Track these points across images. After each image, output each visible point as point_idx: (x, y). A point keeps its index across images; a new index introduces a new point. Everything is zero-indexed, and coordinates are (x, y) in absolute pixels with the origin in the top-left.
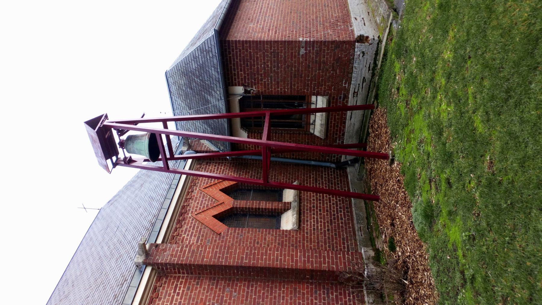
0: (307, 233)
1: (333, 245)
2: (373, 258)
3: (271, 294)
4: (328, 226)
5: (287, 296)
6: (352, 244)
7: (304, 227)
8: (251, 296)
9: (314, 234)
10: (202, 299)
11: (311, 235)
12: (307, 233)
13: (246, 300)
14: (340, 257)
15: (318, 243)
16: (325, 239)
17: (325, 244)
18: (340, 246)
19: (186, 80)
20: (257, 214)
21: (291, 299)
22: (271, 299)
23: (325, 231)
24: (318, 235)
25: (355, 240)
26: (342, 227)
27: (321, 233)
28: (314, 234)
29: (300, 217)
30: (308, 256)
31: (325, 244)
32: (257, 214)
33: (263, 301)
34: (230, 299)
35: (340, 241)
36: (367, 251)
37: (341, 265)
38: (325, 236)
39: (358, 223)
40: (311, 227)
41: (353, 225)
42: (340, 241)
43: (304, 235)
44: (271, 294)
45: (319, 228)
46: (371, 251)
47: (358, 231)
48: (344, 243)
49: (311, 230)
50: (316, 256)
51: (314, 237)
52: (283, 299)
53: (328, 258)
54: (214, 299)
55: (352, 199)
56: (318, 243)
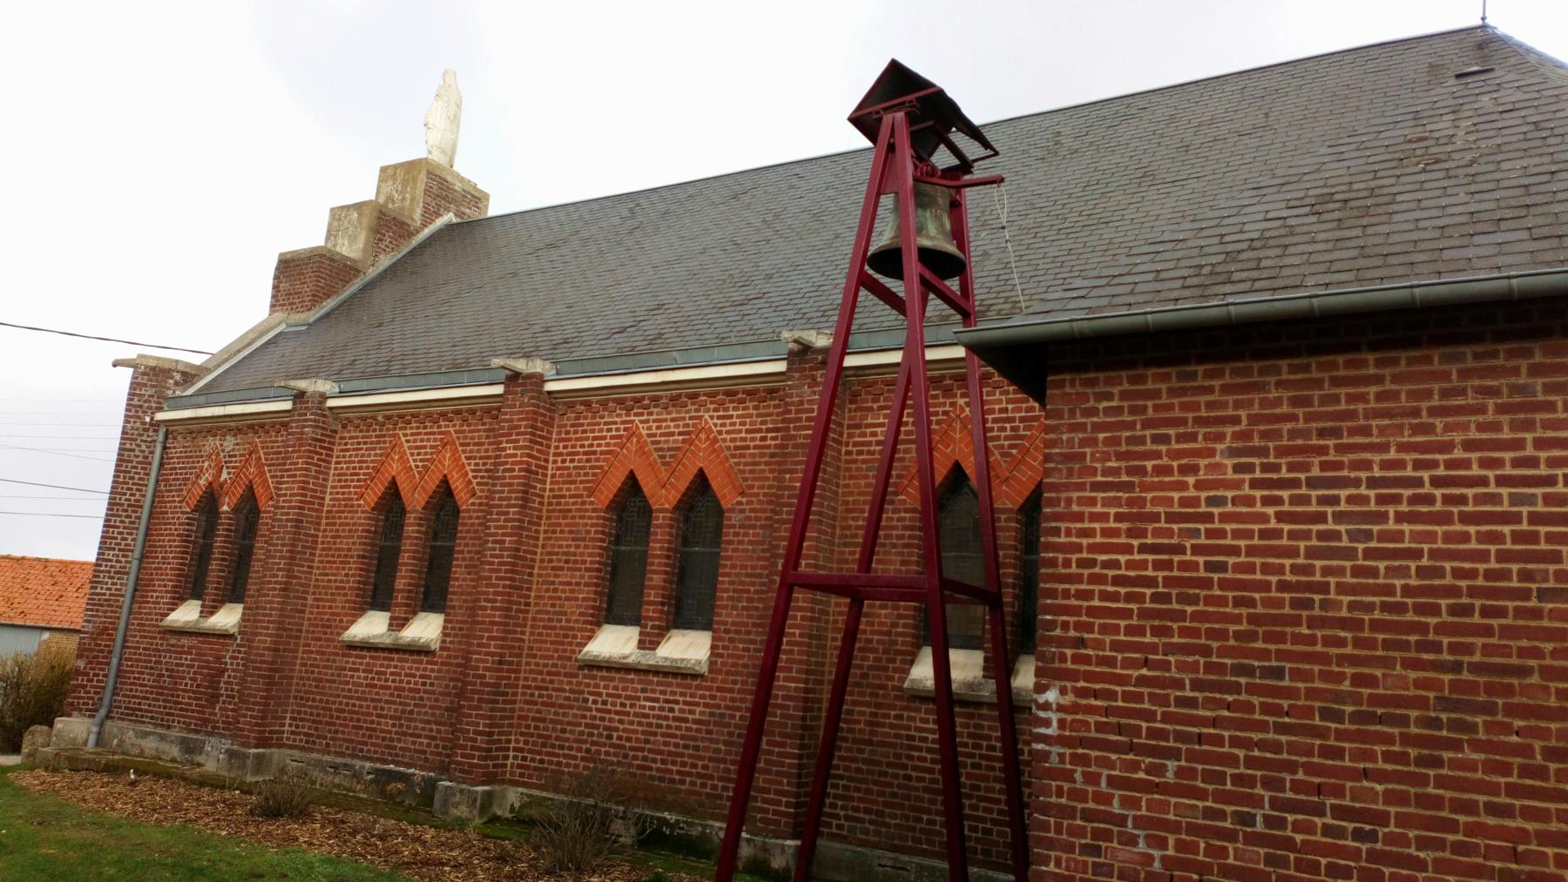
0: (900, 717)
1: (864, 781)
2: (766, 862)
3: (754, 625)
4: (919, 779)
5: (750, 657)
6: (866, 832)
7: (918, 710)
8: (753, 584)
9: (897, 736)
10: (752, 487)
11: (891, 726)
12: (900, 717)
13: (747, 575)
14: (780, 783)
15: (870, 743)
16: (879, 763)
17: (865, 761)
18: (860, 800)
19: (862, 120)
20: (202, 557)
21: (745, 666)
22: (746, 624)
23: (905, 767)
24: (894, 746)
25: (876, 846)
26: (919, 820)
27: (898, 756)
28: (897, 736)
29: (383, 650)
30: (788, 707)
31: (865, 761)
32: (202, 557)
33: (744, 608)
34: (750, 542)
35: (875, 802)
36: (783, 851)
37: (765, 781)
38: (889, 765)
39: (919, 866)
40: (917, 729)
41: (924, 853)
42: (875, 802)
43: (894, 707)
44: (754, 625)
45: (916, 754)
46: (784, 864)
47: (895, 859)
48: (867, 811)
49: (909, 728)
50: (785, 725)
51: (888, 735)
52: (744, 649)
53: (780, 754)
54: (752, 510)
55: (798, 843)
56: (870, 743)
